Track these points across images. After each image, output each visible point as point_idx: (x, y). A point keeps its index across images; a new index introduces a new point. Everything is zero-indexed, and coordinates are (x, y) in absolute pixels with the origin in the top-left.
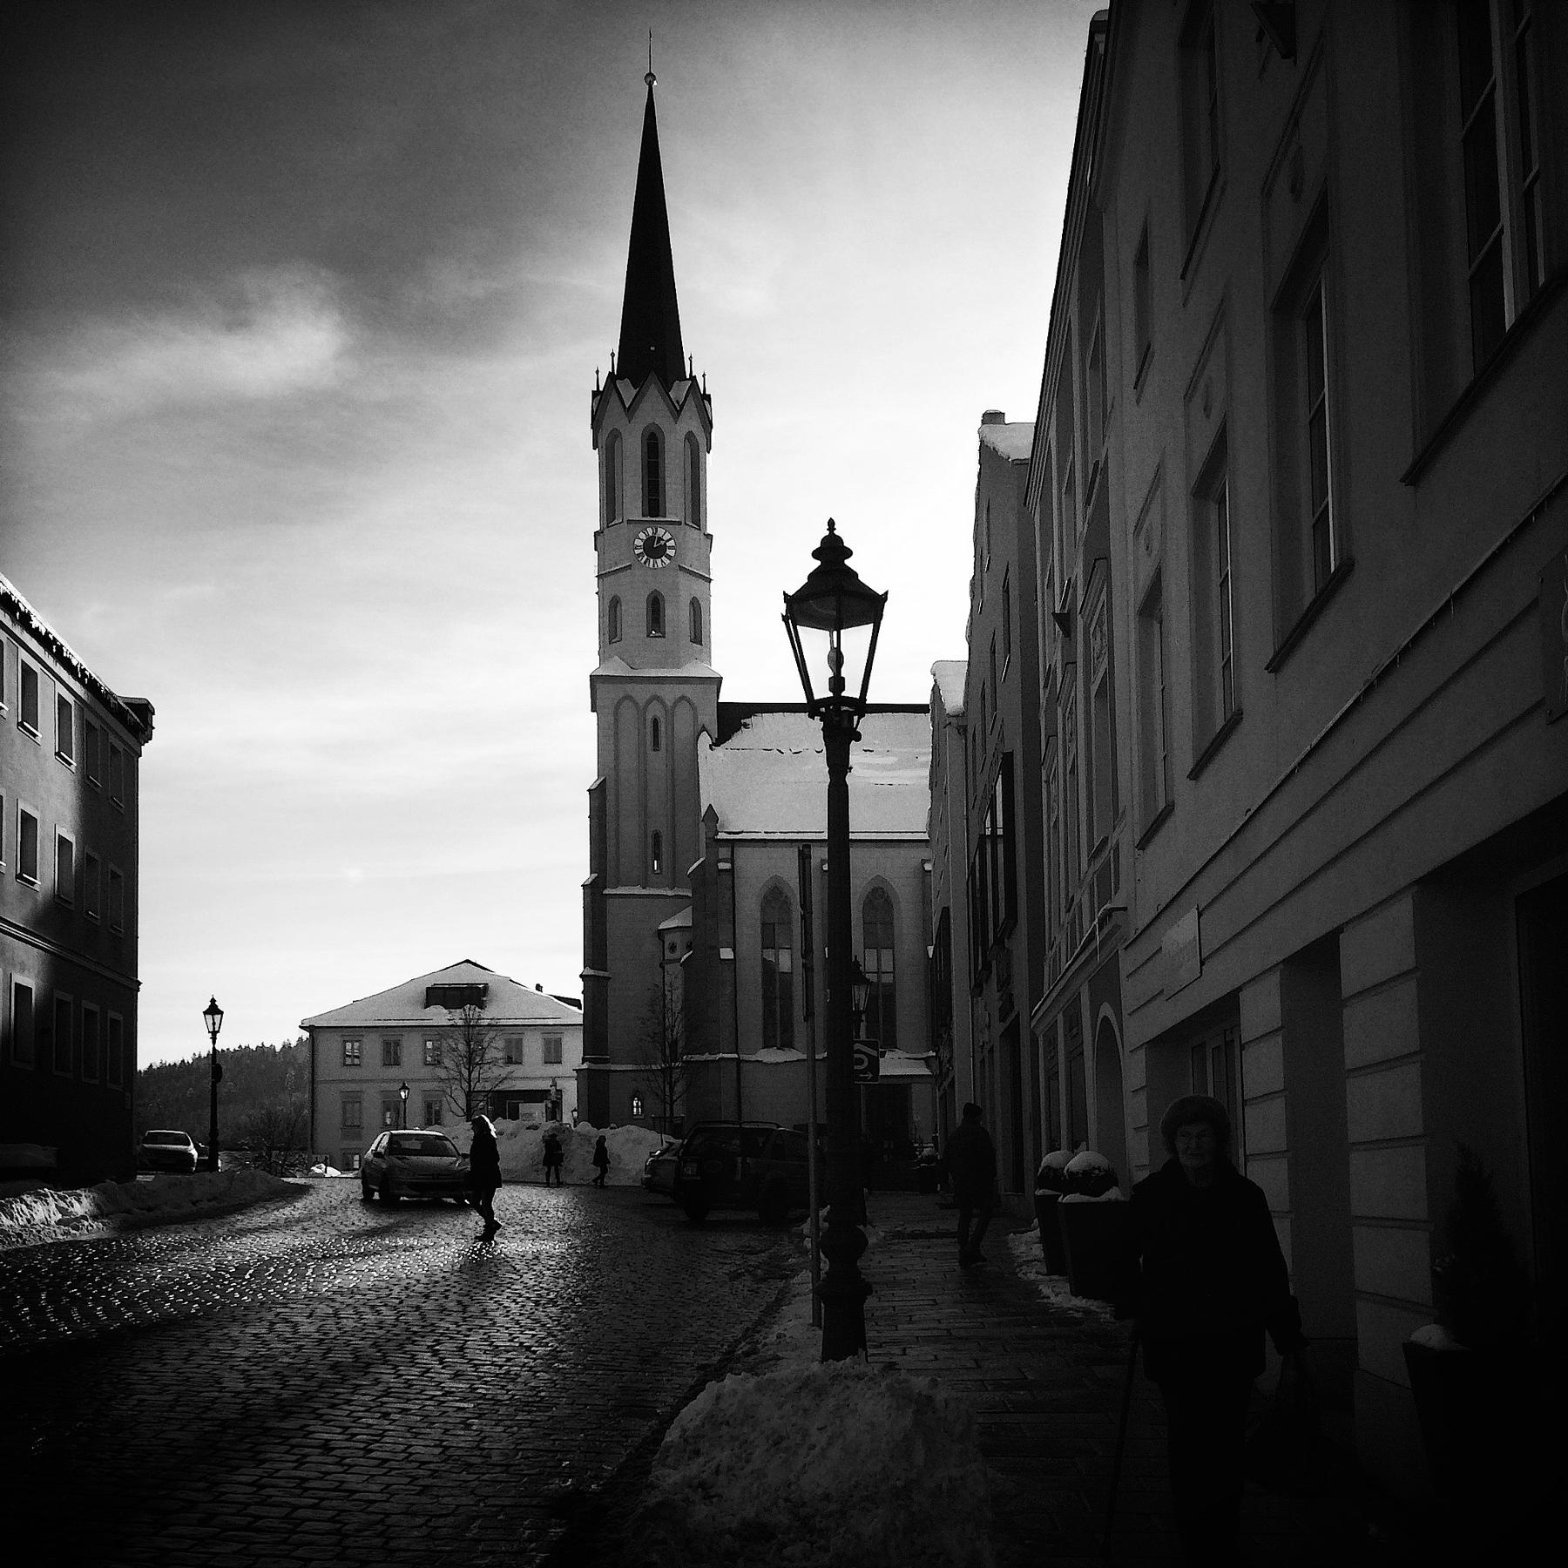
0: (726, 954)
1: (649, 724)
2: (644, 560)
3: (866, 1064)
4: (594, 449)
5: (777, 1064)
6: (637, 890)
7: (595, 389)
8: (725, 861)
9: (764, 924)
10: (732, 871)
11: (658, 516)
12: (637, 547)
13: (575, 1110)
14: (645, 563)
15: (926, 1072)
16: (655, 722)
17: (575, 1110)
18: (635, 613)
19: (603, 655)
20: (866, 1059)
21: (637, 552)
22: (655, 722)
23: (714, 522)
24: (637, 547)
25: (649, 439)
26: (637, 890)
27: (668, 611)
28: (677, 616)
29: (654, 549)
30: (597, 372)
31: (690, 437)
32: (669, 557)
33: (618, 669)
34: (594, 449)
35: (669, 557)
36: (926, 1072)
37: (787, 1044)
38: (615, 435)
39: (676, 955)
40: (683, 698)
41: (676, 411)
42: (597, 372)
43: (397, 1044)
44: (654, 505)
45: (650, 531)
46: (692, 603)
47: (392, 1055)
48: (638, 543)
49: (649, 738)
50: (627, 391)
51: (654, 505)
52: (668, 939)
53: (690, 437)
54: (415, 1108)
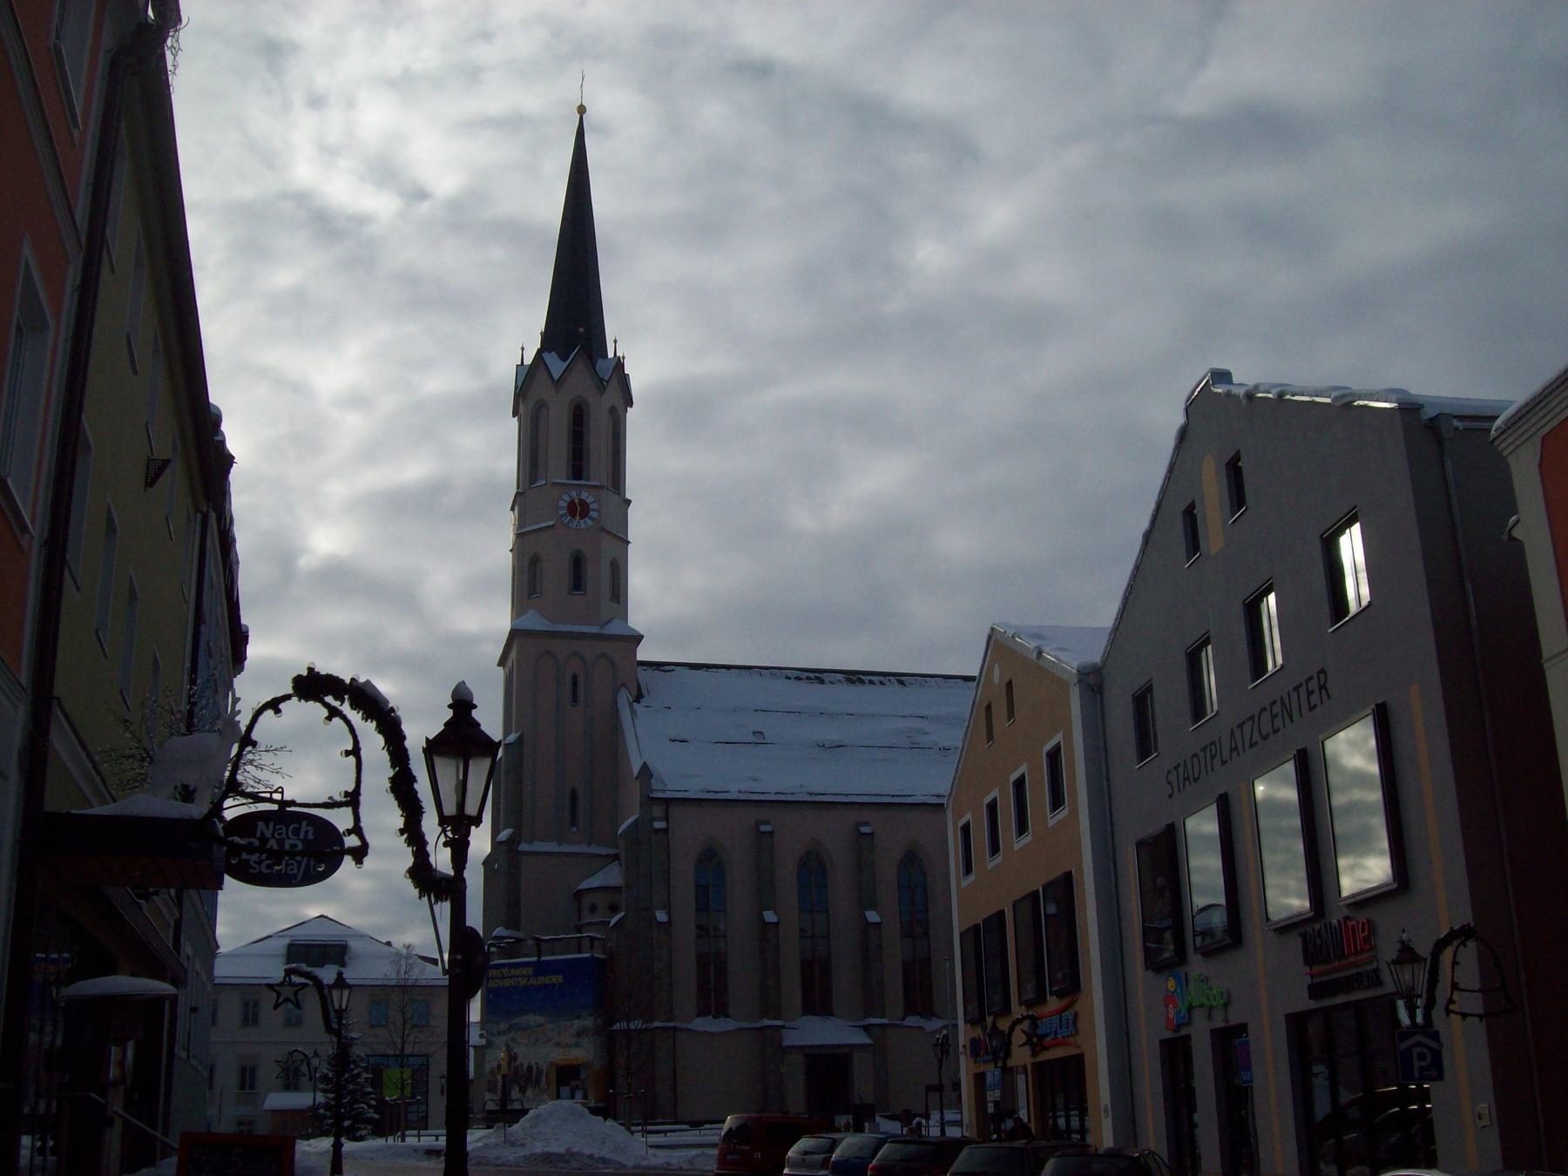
0: (661, 916)
1: (568, 680)
2: (568, 520)
3: (1429, 1060)
4: (514, 416)
5: (712, 1034)
6: (552, 847)
7: (520, 363)
8: (659, 819)
9: (698, 887)
10: (666, 831)
11: (580, 479)
12: (561, 508)
13: (443, 1077)
14: (568, 523)
15: (866, 1040)
16: (575, 678)
17: (443, 1077)
18: (556, 572)
19: (518, 607)
20: (1429, 1056)
21: (561, 512)
22: (575, 678)
23: (632, 489)
24: (561, 508)
25: (575, 410)
26: (552, 847)
27: (590, 570)
28: (598, 575)
29: (578, 509)
30: (523, 349)
31: (613, 410)
32: (593, 519)
33: (534, 621)
34: (514, 416)
35: (593, 519)
36: (866, 1040)
37: (721, 1011)
38: (541, 406)
39: (596, 919)
40: (603, 655)
41: (601, 385)
42: (523, 349)
43: (256, 1005)
44: (578, 468)
45: (574, 494)
46: (612, 565)
47: (250, 1017)
48: (563, 504)
49: (568, 691)
50: (556, 366)
51: (578, 468)
52: (587, 900)
53: (613, 410)
54: (268, 1071)
